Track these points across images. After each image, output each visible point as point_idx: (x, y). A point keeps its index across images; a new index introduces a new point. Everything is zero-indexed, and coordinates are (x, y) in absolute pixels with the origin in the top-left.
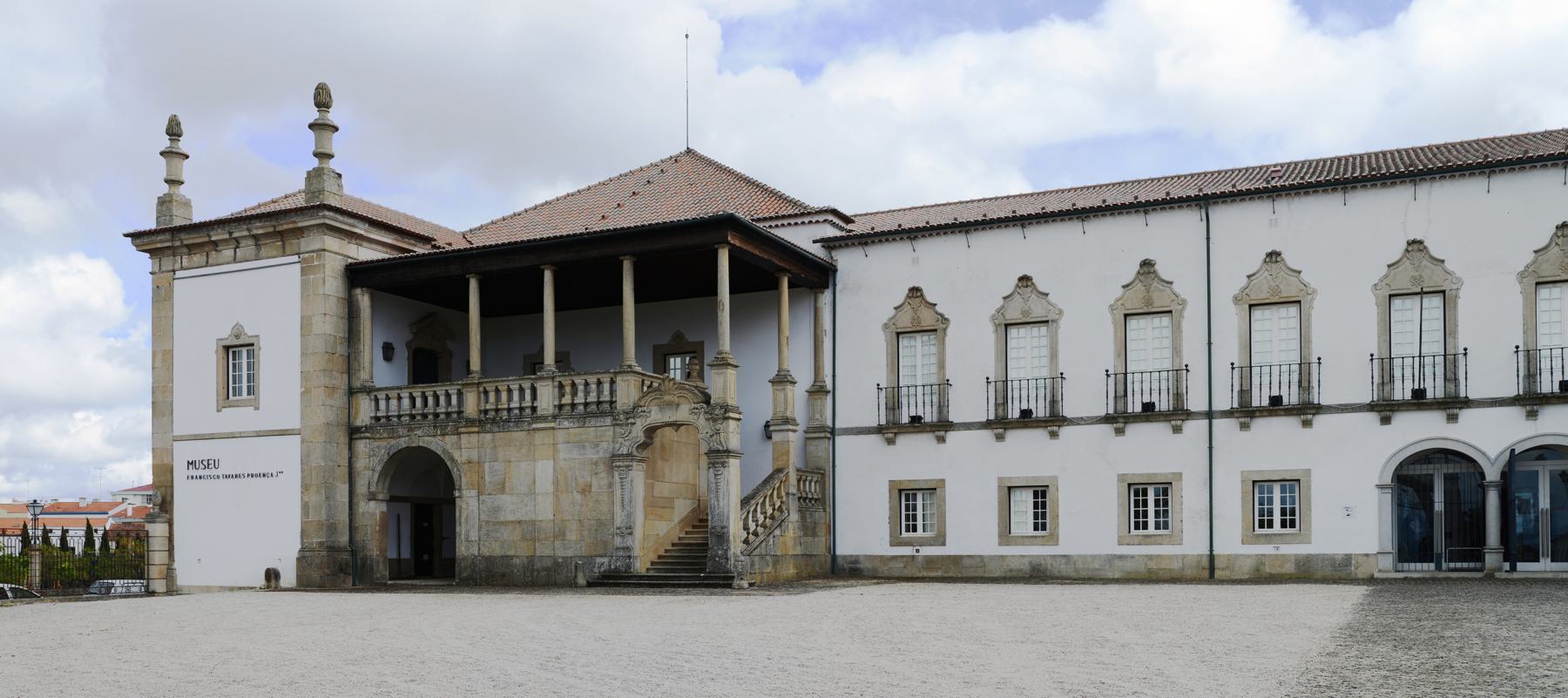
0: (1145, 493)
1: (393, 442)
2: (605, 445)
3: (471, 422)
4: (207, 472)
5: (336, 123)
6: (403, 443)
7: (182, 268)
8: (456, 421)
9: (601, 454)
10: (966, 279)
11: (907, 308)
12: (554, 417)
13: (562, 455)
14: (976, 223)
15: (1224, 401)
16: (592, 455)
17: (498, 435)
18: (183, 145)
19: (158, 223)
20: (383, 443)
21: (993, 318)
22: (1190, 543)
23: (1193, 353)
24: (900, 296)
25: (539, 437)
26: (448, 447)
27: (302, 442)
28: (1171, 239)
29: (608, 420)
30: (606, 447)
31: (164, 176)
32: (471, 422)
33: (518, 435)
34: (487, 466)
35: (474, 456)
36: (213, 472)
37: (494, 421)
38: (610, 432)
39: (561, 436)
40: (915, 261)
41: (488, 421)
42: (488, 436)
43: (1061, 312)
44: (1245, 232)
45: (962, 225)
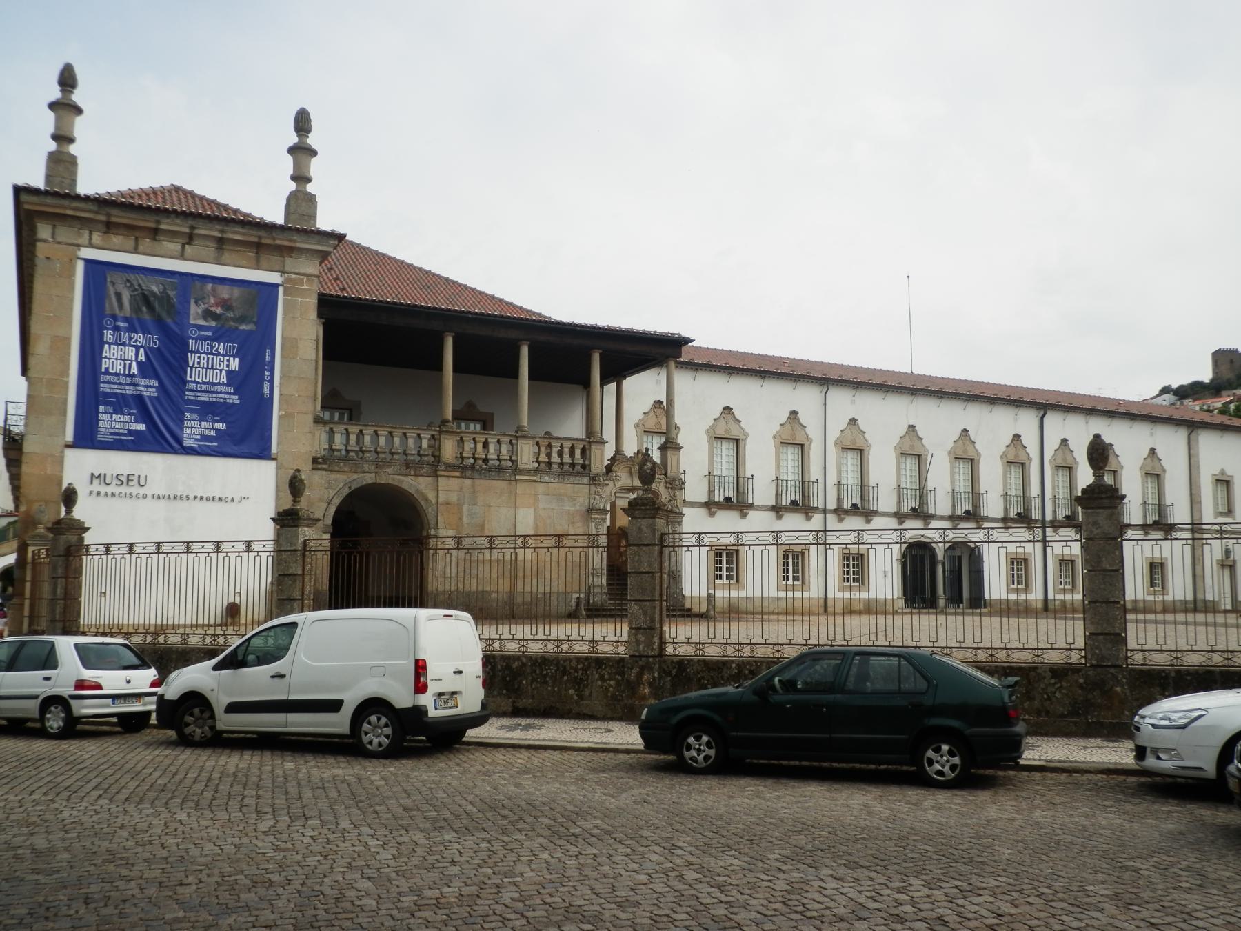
0: (721, 555)
1: (355, 476)
2: (581, 500)
3: (450, 467)
4: (124, 489)
5: (80, 104)
6: (369, 478)
7: (91, 246)
8: (436, 466)
9: (578, 507)
10: (762, 408)
11: (788, 426)
12: (537, 471)
13: (541, 506)
14: (864, 383)
15: (832, 505)
16: (568, 507)
17: (478, 482)
18: (77, 97)
19: (49, 178)
20: (343, 477)
21: (708, 431)
22: (1035, 596)
23: (1034, 490)
24: (1008, 440)
25: (520, 487)
26: (422, 487)
27: (278, 468)
28: (805, 399)
29: (586, 480)
30: (582, 502)
31: (51, 130)
32: (450, 467)
33: (499, 484)
34: (465, 508)
35: (454, 498)
36: (135, 490)
37: (473, 467)
38: (586, 489)
39: (541, 488)
40: (1016, 420)
41: (463, 468)
42: (468, 482)
43: (747, 435)
44: (843, 404)
45: (764, 372)
